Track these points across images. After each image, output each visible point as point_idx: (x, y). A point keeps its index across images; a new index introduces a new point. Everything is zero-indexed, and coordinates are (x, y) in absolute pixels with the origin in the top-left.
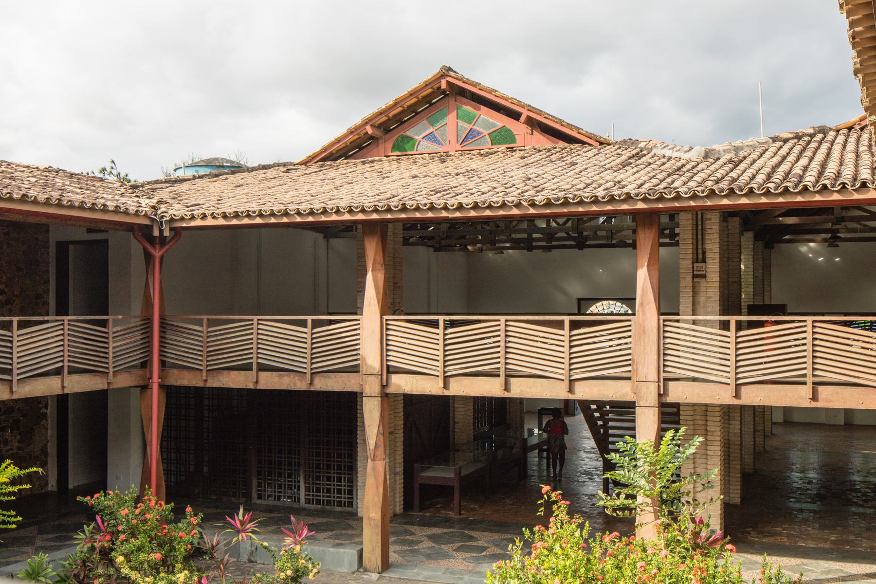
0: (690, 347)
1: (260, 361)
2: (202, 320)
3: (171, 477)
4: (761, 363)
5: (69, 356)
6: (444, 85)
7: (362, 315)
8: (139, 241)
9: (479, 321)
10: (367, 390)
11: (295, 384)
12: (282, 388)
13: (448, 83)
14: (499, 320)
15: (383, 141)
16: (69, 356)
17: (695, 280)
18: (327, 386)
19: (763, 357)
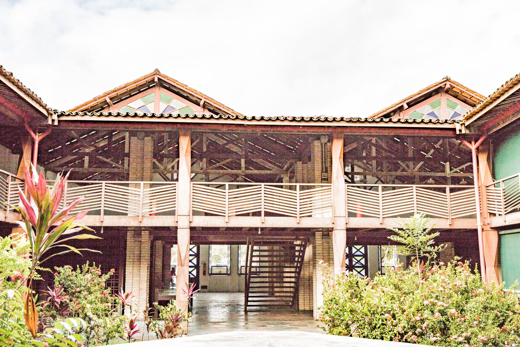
0: (108, 192)
1: (194, 209)
2: (445, 188)
3: (246, 272)
4: (369, 207)
5: (225, 207)
6: (156, 80)
7: (331, 183)
8: (331, 159)
9: (92, 184)
10: (179, 225)
11: (130, 223)
12: (121, 225)
13: (159, 79)
14: (102, 183)
15: (113, 108)
16: (225, 207)
17: (327, 136)
18: (152, 223)
19: (406, 196)
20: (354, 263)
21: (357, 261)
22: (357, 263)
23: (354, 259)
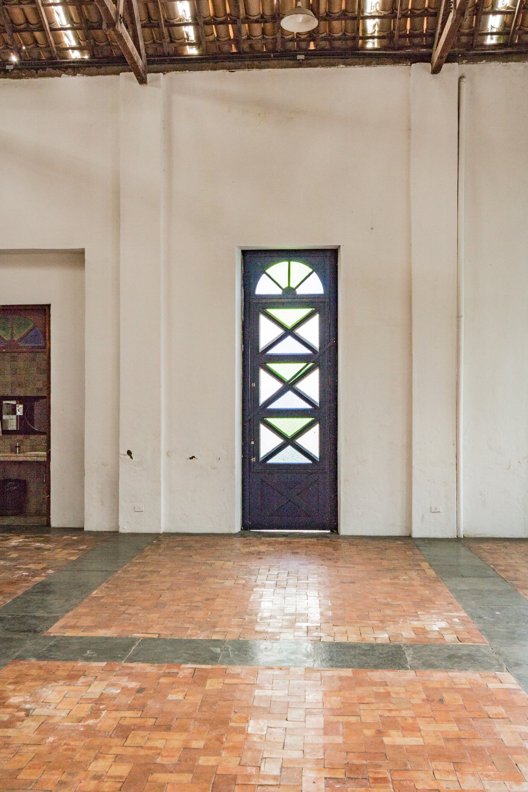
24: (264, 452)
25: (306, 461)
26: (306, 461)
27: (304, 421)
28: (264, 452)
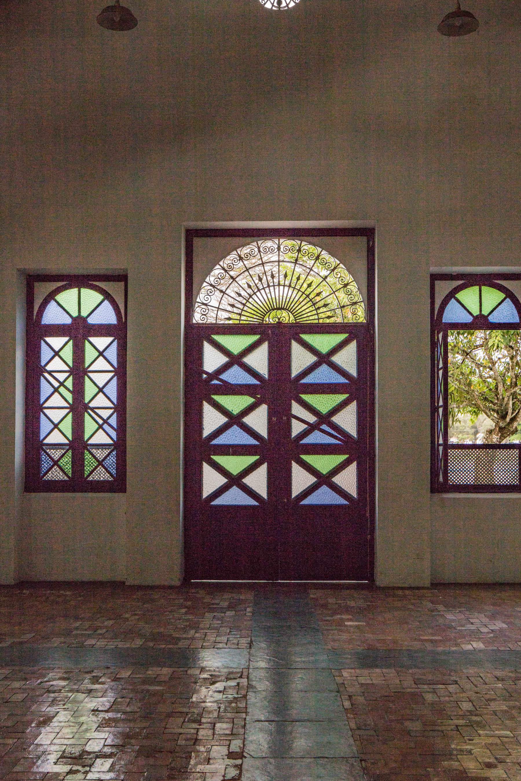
20: (297, 428)
21: (312, 419)
22: (312, 428)
23: (296, 409)
24: (296, 491)
25: (253, 502)
26: (253, 502)
27: (251, 460)
28: (296, 491)
